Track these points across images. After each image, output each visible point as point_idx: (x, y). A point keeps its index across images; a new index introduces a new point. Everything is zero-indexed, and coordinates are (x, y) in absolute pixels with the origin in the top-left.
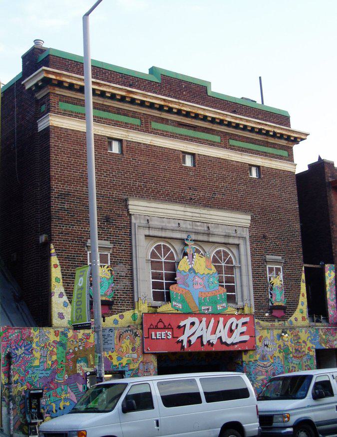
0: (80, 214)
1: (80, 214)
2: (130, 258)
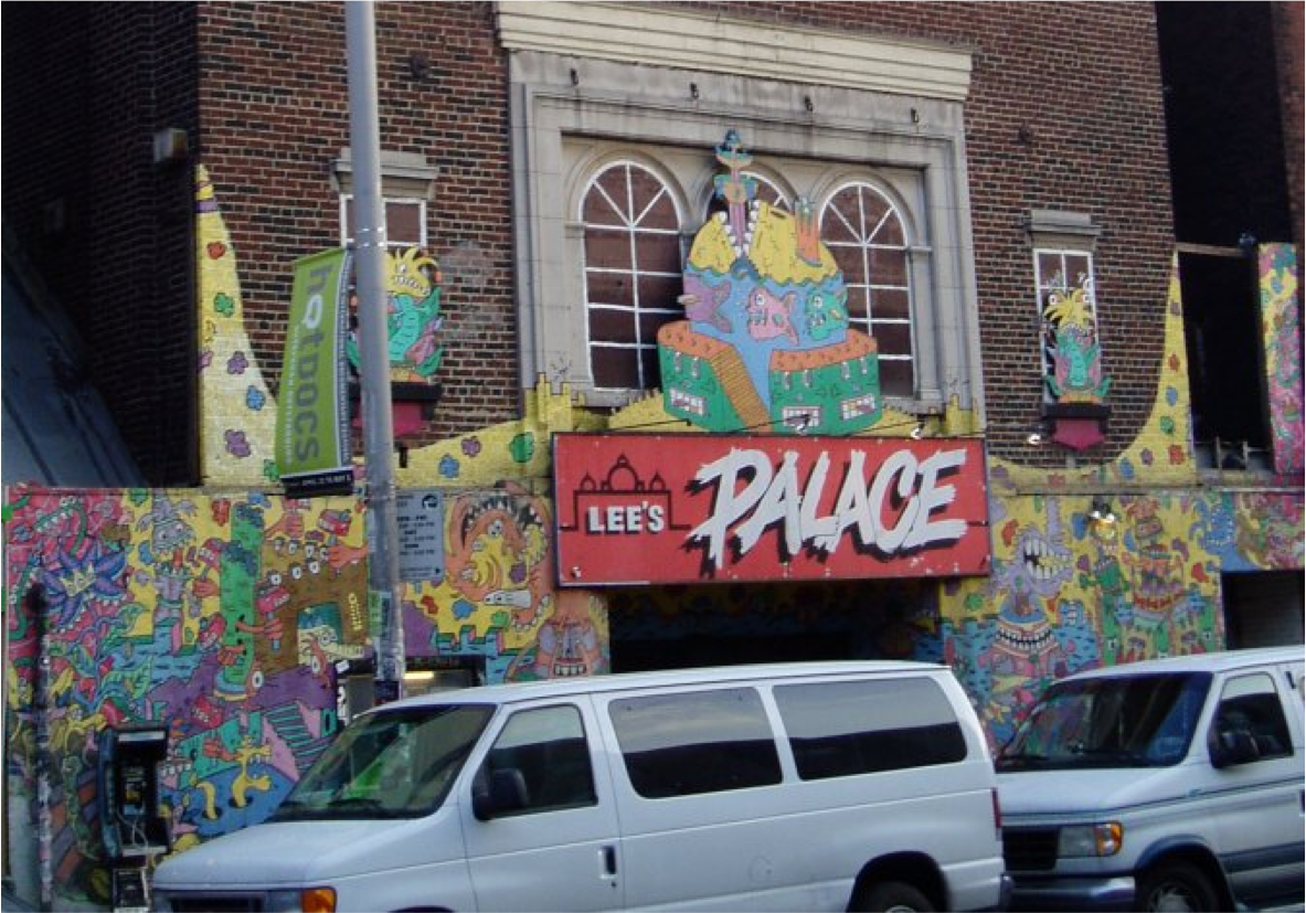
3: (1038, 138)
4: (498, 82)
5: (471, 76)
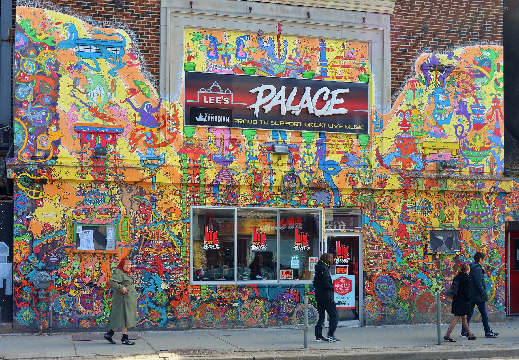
2: (156, 63)
3: (430, 30)
4: (156, 7)
5: (143, 5)
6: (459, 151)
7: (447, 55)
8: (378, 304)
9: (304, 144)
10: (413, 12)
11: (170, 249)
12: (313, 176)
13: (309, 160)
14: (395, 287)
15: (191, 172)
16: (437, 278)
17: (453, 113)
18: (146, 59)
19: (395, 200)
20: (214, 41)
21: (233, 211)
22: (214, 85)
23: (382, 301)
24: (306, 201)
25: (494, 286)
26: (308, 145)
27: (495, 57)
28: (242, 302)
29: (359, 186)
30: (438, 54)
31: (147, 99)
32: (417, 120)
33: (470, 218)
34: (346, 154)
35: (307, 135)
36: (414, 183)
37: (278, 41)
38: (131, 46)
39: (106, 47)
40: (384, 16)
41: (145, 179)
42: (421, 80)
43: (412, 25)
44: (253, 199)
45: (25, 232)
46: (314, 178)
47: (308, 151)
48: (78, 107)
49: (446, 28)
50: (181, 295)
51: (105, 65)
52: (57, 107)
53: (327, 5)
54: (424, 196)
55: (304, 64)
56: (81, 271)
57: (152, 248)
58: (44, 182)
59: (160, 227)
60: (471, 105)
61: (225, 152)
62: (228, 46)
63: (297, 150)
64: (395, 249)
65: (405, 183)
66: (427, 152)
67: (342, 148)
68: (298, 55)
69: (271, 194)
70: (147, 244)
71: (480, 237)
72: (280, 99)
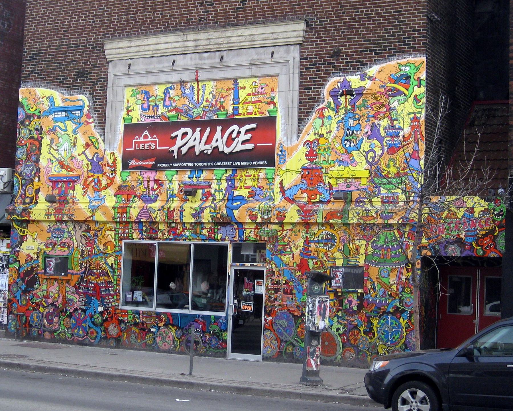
0: (50, 74)
1: (50, 74)
3: (343, 53)
6: (370, 178)
7: (359, 77)
8: (277, 340)
9: (167, 182)
10: (325, 37)
11: (106, 278)
12: (217, 212)
13: (219, 196)
14: (295, 324)
15: (120, 211)
16: (338, 317)
17: (364, 138)
18: (98, 117)
19: (298, 233)
20: (147, 94)
21: (153, 245)
22: (145, 133)
23: (280, 337)
24: (213, 235)
25: (404, 330)
26: (219, 181)
27: (415, 71)
28: (159, 327)
29: (259, 220)
30: (350, 77)
31: (96, 151)
32: (325, 149)
33: (378, 252)
34: (253, 189)
35: (219, 172)
36: (314, 215)
37: (198, 86)
38: (88, 108)
39: (71, 111)
40: (292, 47)
41: (88, 218)
42: (329, 106)
43: (323, 51)
44: (169, 234)
45: (16, 261)
46: (217, 214)
47: (219, 187)
48: (52, 162)
49: (359, 48)
50: (112, 317)
51: (71, 126)
52: (40, 163)
53: (240, 46)
54: (327, 229)
55: (219, 105)
56: (47, 293)
57: (93, 276)
58: (28, 222)
59: (99, 258)
60: (385, 128)
61: (151, 192)
62: (158, 97)
63: (210, 187)
64: (295, 284)
65: (304, 216)
66: (333, 182)
67: (249, 183)
68: (214, 97)
69: (184, 229)
70: (91, 273)
71: (389, 275)
72: (195, 140)
